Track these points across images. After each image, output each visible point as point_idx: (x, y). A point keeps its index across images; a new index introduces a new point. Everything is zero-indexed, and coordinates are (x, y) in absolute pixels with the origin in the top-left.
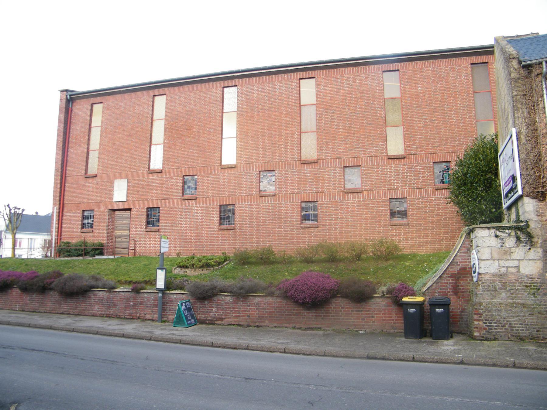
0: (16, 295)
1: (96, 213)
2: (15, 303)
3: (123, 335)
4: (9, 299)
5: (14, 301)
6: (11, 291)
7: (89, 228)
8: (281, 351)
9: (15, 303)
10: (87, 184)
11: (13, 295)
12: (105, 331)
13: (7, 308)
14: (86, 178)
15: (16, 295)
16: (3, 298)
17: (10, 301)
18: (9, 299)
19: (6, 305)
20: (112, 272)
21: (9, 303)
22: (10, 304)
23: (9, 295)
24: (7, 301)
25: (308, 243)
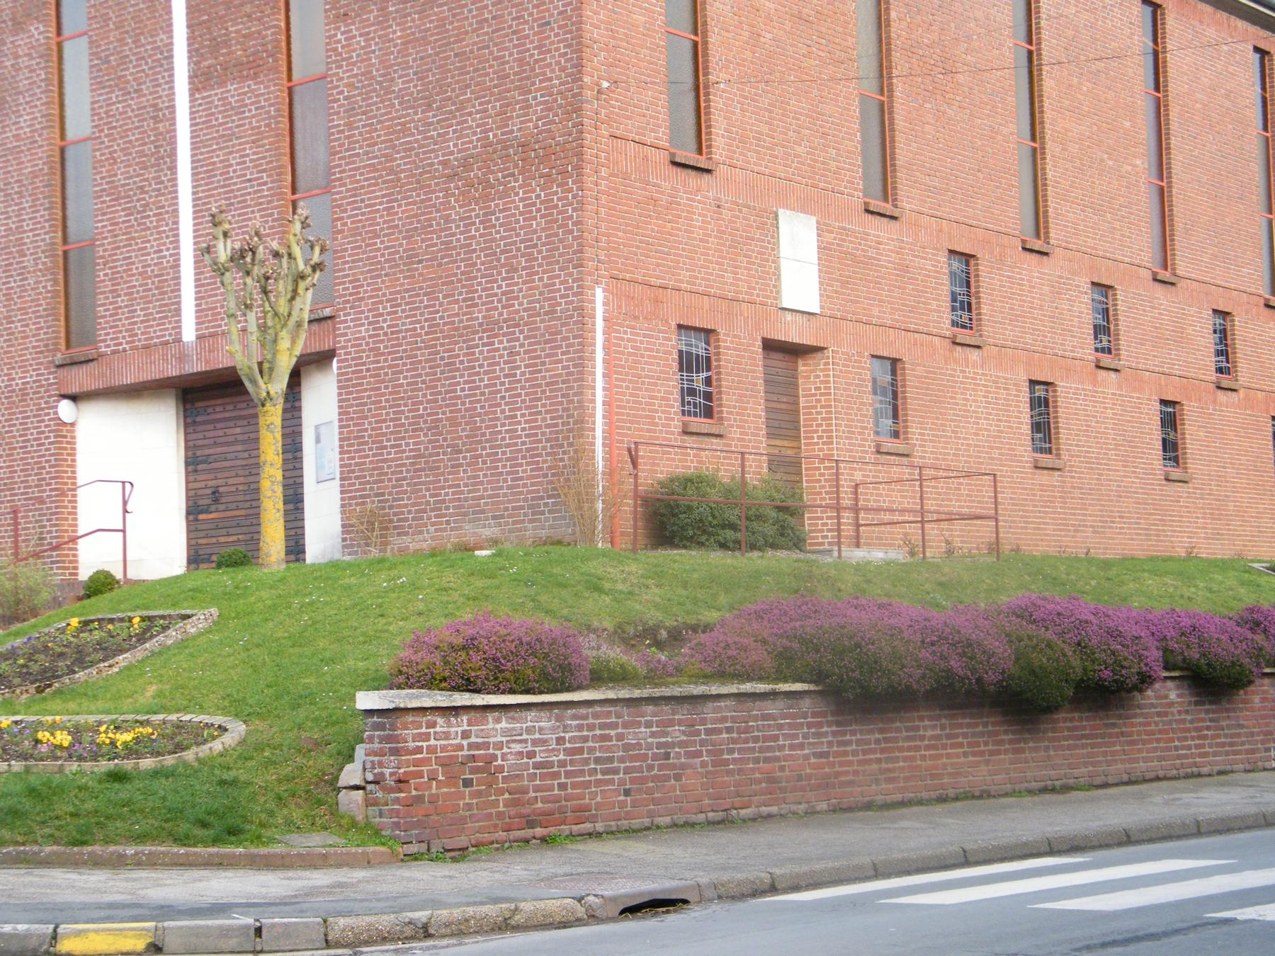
0: (1264, 708)
1: (726, 341)
2: (1263, 742)
3: (1128, 836)
4: (1242, 726)
5: (1258, 734)
6: (1246, 694)
7: (695, 415)
8: (1042, 849)
9: (1263, 742)
10: (683, 198)
11: (1252, 709)
12: (805, 868)
13: (1241, 766)
14: (674, 168)
15: (1264, 708)
16: (1224, 723)
17: (1246, 735)
18: (1242, 726)
19: (1235, 753)
20: (961, 607)
21: (1243, 744)
22: (1247, 747)
23: (1241, 710)
24: (1239, 735)
25: (820, 450)
